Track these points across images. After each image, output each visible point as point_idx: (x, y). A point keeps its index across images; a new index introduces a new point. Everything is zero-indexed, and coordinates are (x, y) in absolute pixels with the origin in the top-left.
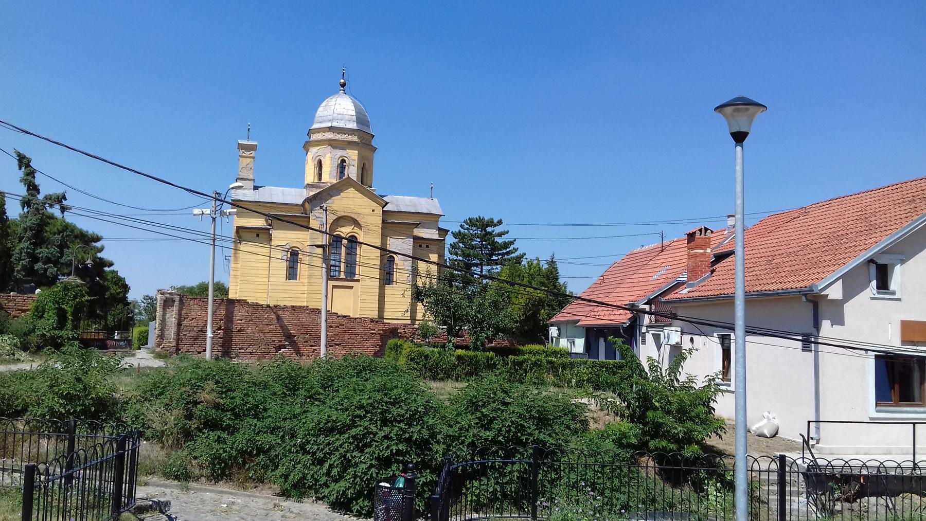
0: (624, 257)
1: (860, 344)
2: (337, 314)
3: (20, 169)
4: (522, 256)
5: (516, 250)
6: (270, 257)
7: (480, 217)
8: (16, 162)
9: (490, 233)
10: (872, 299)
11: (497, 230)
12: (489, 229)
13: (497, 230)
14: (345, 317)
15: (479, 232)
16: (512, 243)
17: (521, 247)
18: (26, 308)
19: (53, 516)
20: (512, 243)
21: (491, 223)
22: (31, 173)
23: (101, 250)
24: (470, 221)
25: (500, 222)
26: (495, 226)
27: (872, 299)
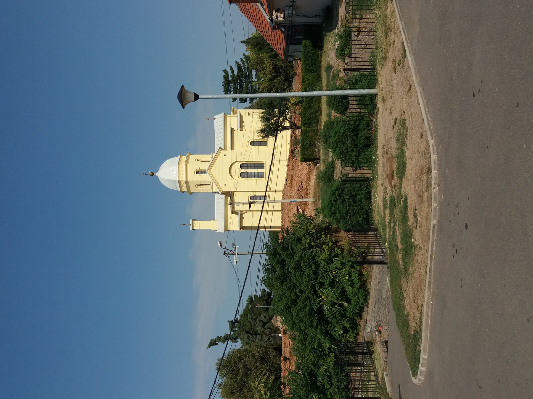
0: (242, 13)
1: (264, 235)
2: (285, 185)
3: (217, 344)
4: (244, 54)
5: (242, 60)
6: (252, 254)
7: (223, 85)
8: (215, 346)
9: (233, 77)
10: (253, 143)
11: (230, 73)
12: (230, 78)
13: (230, 73)
14: (286, 180)
15: (232, 84)
16: (238, 63)
17: (239, 57)
18: (289, 342)
19: (372, 392)
20: (238, 63)
21: (226, 77)
22: (219, 339)
23: (255, 296)
24: (226, 91)
25: (225, 71)
26: (228, 75)
27: (253, 143)
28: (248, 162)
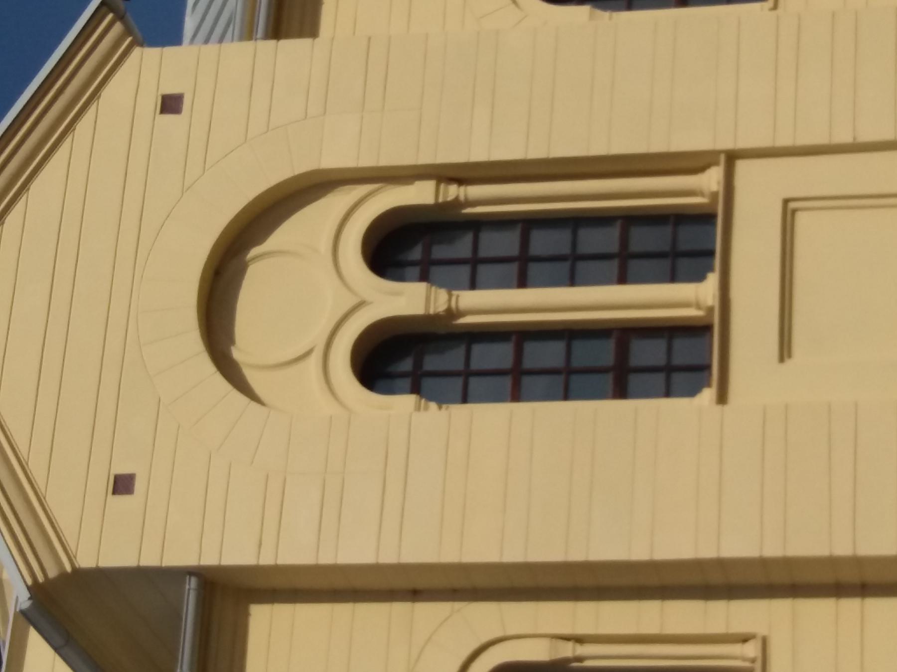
28: (475, 191)
